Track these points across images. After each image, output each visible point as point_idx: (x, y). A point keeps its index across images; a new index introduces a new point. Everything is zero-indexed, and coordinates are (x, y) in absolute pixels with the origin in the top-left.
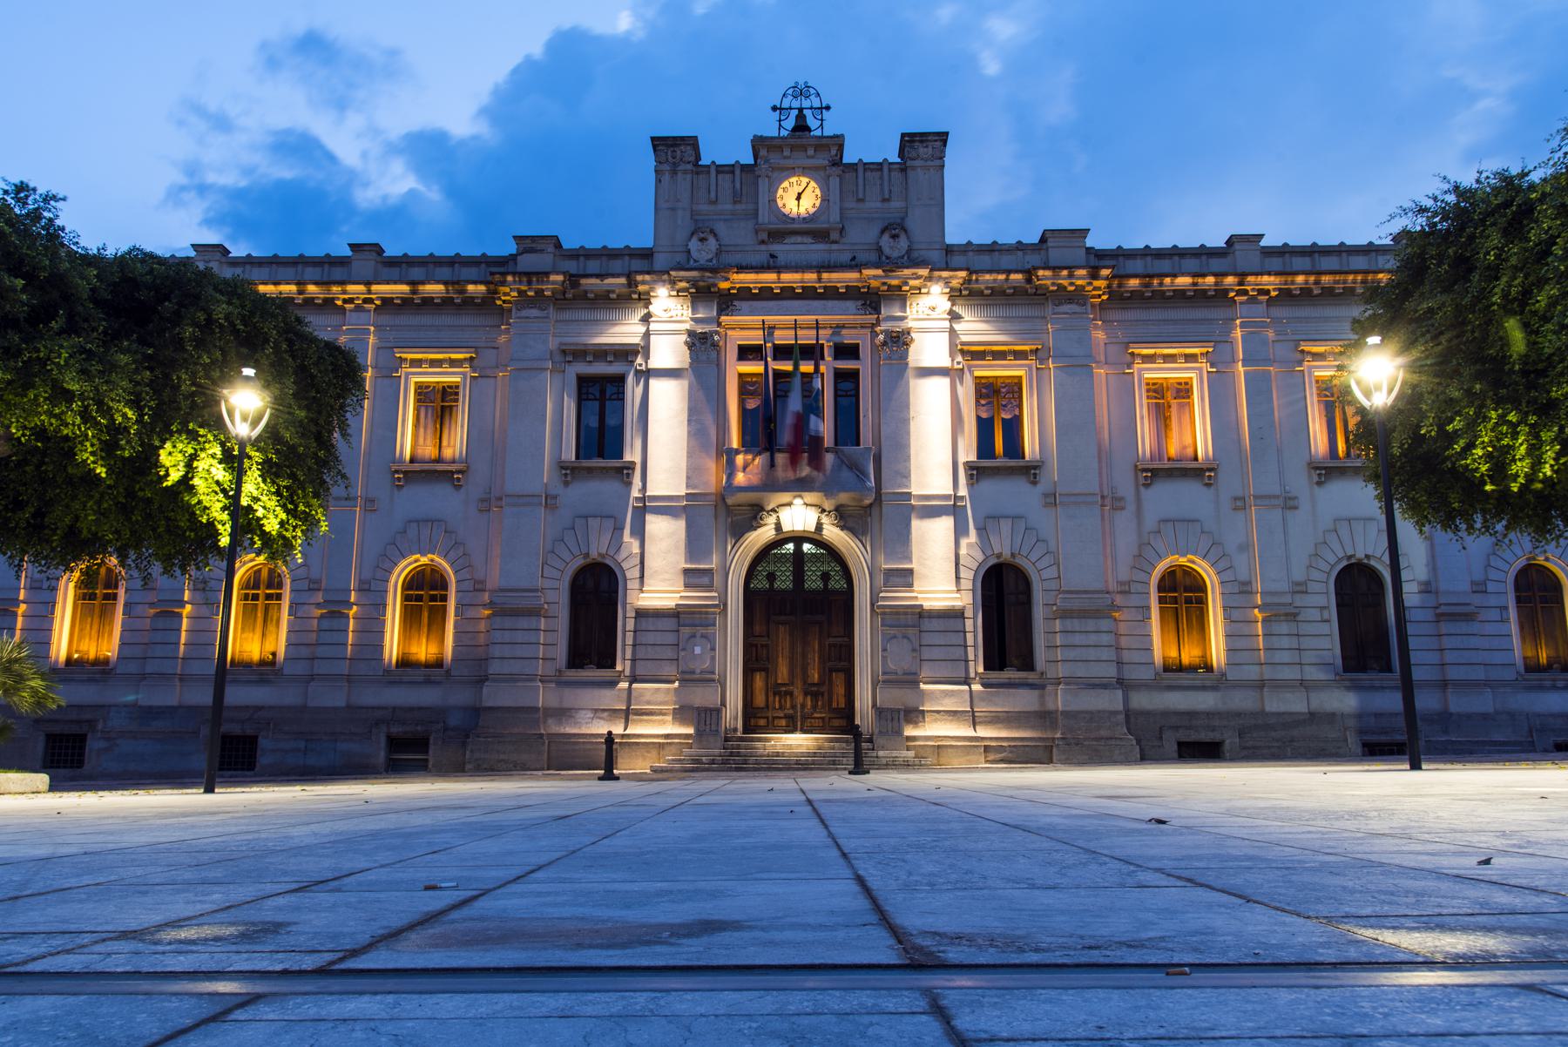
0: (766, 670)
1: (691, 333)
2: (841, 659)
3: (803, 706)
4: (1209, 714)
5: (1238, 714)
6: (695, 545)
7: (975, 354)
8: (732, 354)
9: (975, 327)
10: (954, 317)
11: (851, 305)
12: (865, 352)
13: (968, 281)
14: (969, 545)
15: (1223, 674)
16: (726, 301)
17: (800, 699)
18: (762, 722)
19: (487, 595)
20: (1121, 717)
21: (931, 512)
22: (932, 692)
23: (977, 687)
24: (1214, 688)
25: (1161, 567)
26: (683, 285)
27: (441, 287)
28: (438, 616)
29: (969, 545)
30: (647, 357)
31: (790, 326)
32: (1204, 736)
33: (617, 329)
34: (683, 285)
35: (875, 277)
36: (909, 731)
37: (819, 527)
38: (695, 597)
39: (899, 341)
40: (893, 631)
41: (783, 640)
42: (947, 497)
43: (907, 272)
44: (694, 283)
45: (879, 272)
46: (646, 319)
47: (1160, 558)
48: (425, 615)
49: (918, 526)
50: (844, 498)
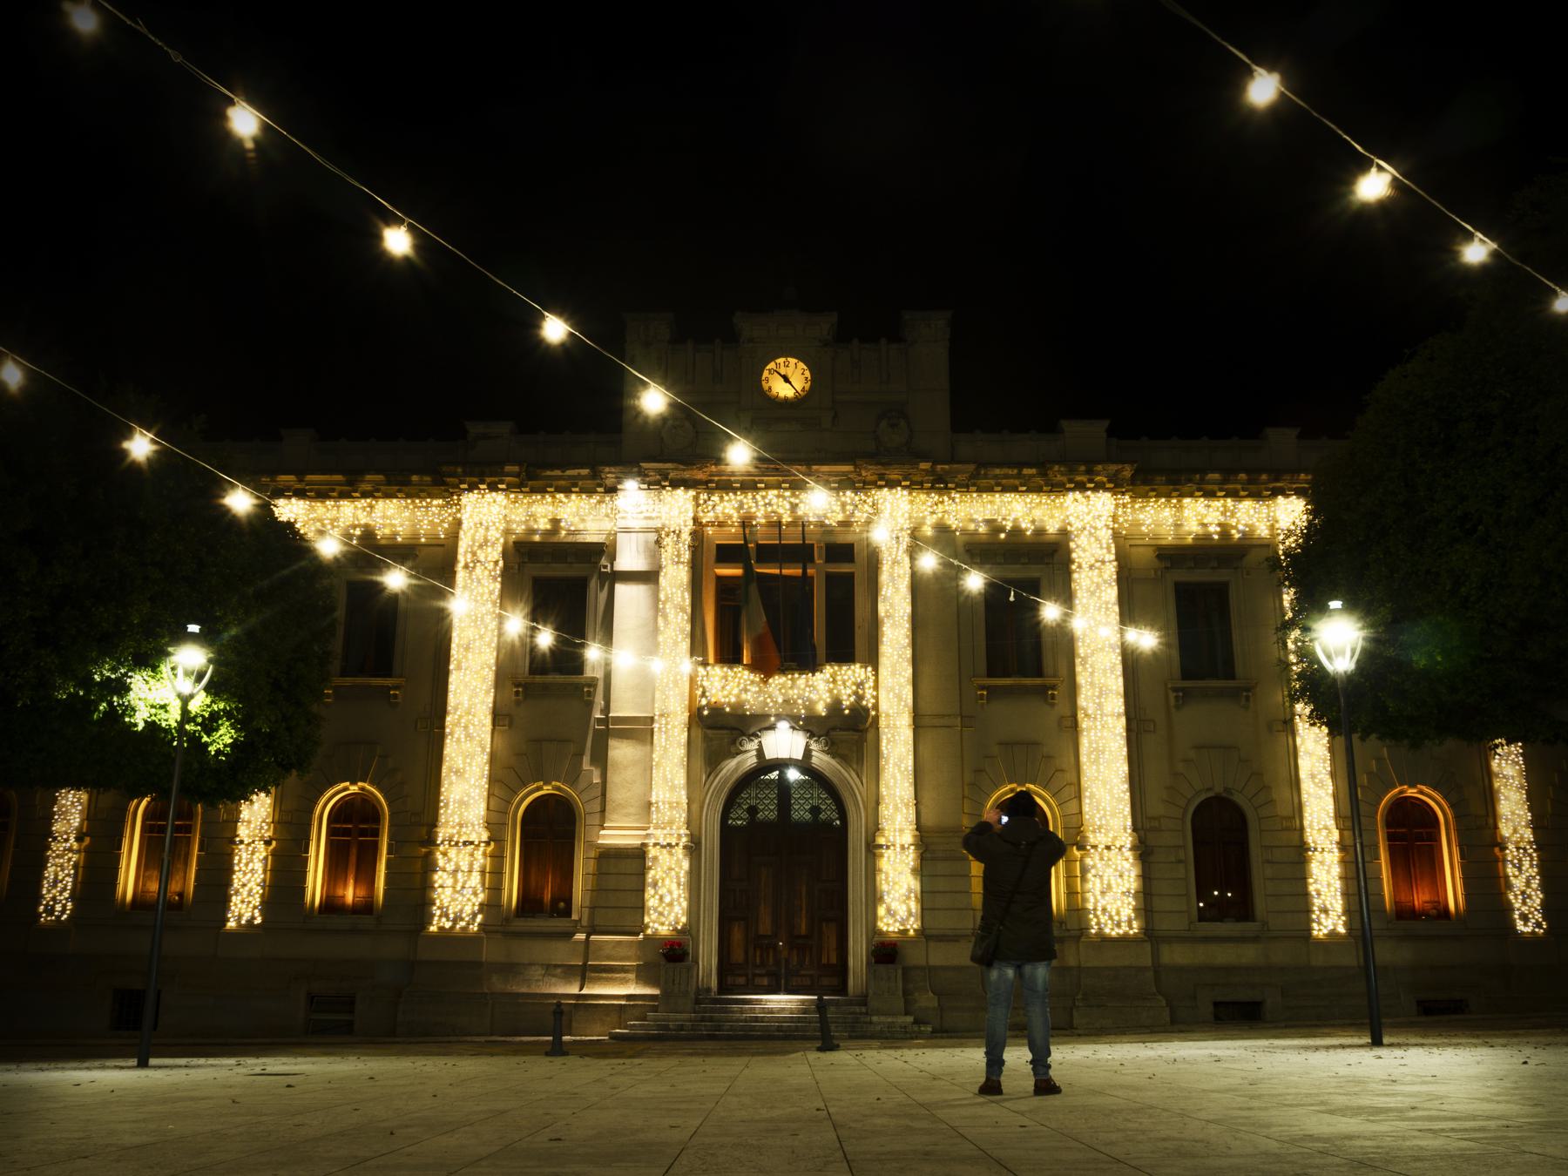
17: (785, 954)
18: (741, 980)
20: (1150, 974)
24: (1255, 939)
32: (1244, 995)
37: (808, 753)
48: (354, 851)
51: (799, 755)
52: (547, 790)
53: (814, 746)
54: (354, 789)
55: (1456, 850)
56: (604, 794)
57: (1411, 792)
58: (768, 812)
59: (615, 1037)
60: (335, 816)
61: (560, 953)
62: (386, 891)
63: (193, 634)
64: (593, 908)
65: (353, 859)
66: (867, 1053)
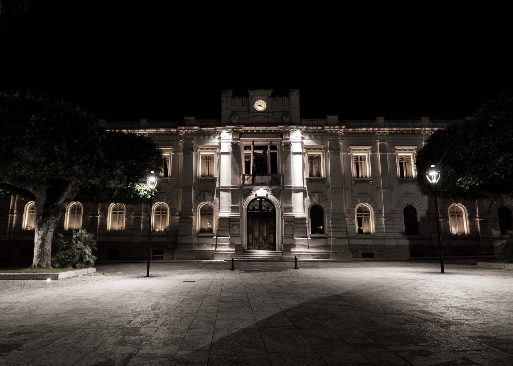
0: (252, 233)
1: (232, 143)
2: (272, 231)
3: (262, 243)
4: (370, 245)
5: (379, 245)
6: (234, 200)
7: (308, 149)
8: (243, 148)
9: (308, 141)
10: (303, 138)
11: (275, 135)
12: (279, 148)
13: (306, 129)
14: (307, 200)
15: (374, 235)
16: (241, 134)
18: (251, 247)
19: (178, 213)
20: (348, 247)
21: (297, 191)
22: (298, 240)
23: (309, 238)
24: (372, 239)
25: (358, 206)
26: (230, 130)
27: (164, 130)
28: (164, 218)
29: (307, 200)
30: (220, 149)
31: (259, 141)
32: (369, 252)
33: (212, 141)
34: (230, 130)
35: (282, 128)
36: (292, 250)
37: (267, 195)
38: (234, 214)
39: (288, 145)
40: (287, 223)
41: (257, 225)
42: (301, 187)
43: (290, 127)
44: (233, 129)
45: (283, 127)
46: (220, 138)
47: (357, 204)
48: (161, 217)
49: (294, 195)
50: (274, 187)
51: (265, 196)
52: (206, 203)
53: (269, 193)
54: (161, 203)
55: (373, 218)
56: (219, 204)
57: (363, 205)
58: (257, 207)
59: (225, 260)
60: (156, 210)
61: (212, 241)
62: (481, 229)
63: (433, 168)
64: (218, 231)
65: (161, 219)
66: (502, 264)
